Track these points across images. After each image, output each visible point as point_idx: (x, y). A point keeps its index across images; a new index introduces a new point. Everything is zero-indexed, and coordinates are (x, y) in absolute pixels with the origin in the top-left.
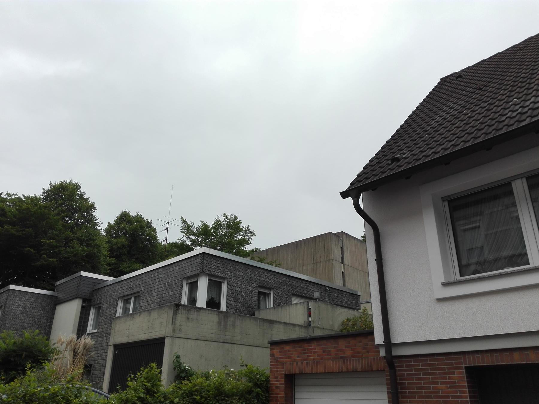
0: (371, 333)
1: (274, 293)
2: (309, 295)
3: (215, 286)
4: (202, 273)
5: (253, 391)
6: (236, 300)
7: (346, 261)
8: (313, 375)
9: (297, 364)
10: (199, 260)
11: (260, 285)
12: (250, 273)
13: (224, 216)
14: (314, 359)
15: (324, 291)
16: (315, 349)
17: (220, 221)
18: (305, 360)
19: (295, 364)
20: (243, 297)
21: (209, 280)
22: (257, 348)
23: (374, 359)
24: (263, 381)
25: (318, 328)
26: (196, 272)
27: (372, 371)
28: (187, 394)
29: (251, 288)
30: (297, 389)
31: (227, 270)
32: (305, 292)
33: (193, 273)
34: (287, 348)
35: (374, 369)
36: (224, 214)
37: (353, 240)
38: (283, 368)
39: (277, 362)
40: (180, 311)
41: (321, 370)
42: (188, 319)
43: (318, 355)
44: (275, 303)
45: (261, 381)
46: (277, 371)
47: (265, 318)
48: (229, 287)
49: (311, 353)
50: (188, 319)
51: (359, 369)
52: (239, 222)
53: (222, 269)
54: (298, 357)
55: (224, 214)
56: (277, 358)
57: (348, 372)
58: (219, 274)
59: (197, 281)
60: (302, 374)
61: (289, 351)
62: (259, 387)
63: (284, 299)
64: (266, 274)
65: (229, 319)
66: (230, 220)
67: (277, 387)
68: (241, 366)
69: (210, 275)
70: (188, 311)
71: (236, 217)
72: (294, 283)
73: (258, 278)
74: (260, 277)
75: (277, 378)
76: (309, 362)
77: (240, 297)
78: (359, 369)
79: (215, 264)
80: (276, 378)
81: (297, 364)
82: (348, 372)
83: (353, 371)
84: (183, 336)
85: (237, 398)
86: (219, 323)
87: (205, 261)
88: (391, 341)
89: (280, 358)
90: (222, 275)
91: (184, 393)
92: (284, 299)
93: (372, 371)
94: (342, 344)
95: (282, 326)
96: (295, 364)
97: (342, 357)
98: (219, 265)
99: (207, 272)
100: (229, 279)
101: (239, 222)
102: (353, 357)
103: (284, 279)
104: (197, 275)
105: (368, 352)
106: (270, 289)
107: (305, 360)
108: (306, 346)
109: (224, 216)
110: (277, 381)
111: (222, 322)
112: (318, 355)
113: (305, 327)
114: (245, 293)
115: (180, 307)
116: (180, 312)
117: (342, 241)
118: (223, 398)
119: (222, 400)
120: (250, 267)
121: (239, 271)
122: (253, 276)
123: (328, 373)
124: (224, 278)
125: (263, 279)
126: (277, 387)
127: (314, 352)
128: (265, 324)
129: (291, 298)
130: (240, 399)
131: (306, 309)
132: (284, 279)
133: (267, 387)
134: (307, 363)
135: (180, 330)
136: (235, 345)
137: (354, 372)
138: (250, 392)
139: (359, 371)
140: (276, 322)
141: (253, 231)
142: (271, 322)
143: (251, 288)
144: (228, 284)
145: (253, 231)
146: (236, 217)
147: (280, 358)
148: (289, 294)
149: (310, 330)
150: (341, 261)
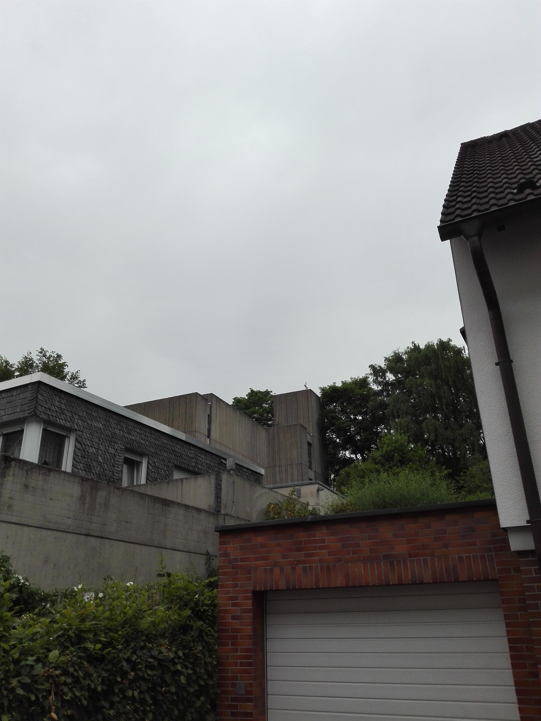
0: (491, 507)
1: (148, 463)
2: (198, 468)
3: (52, 442)
4: (34, 417)
5: (191, 627)
6: (88, 468)
7: (213, 435)
8: (294, 591)
9: (282, 569)
10: (28, 395)
11: (129, 446)
12: (114, 425)
13: (41, 353)
14: (321, 561)
15: (218, 464)
16: (323, 541)
17: (31, 359)
18: (299, 562)
19: (277, 570)
20: (100, 464)
21: (44, 429)
22: (143, 547)
23: (461, 558)
24: (207, 605)
25: (231, 516)
26: (22, 415)
27: (457, 581)
28: (69, 636)
29: (113, 451)
30: (270, 620)
31: (77, 417)
32: (193, 464)
33: (16, 416)
34: (259, 539)
35: (463, 576)
36: (42, 349)
37: (225, 406)
38: (249, 579)
39: (234, 567)
40: (11, 469)
41: (339, 581)
42: (26, 486)
43: (330, 554)
44: (150, 478)
45: (204, 605)
46: (236, 586)
47: (157, 495)
48: (78, 446)
49: (315, 548)
50: (26, 486)
51: (428, 577)
52: (64, 365)
53: (69, 414)
54: (284, 557)
55: (42, 349)
56: (236, 560)
57: (400, 584)
58: (62, 422)
59: (22, 431)
60: (294, 589)
61: (262, 546)
62: (200, 618)
63: (162, 472)
64: (138, 431)
65: (99, 494)
66: (49, 358)
67: (234, 618)
68: (160, 575)
69: (46, 422)
70: (27, 471)
71: (59, 356)
72: (178, 448)
73: (126, 435)
74: (129, 433)
75: (236, 598)
76: (311, 568)
77: (95, 464)
78: (428, 577)
79: (57, 404)
80: (231, 598)
81: (282, 569)
82: (400, 584)
83: (414, 584)
84: (14, 519)
85: (166, 641)
86: (82, 499)
87: (40, 397)
88: (499, 525)
89: (242, 560)
90: (68, 425)
91: (63, 635)
92: (162, 472)
93: (457, 581)
94: (386, 531)
95: (181, 511)
96: (277, 570)
97: (386, 557)
98: (63, 407)
99: (43, 416)
100: (78, 432)
101: (64, 365)
102: (410, 556)
103: (165, 441)
104: (23, 421)
105: (446, 546)
106: (142, 455)
107: (299, 562)
108: (302, 536)
109: (41, 353)
110: (234, 605)
111: (88, 499)
112: (330, 554)
113: (214, 514)
114: (104, 459)
115: (13, 463)
116: (11, 473)
117: (211, 406)
118: (142, 644)
119: (143, 648)
120: (114, 417)
121: (96, 421)
122: (117, 431)
123: (354, 587)
124: (70, 430)
125: (133, 438)
126: (234, 618)
127: (321, 548)
128: (157, 505)
129: (172, 472)
130: (171, 644)
131: (213, 485)
132: (165, 441)
133: (213, 617)
134: (305, 569)
135: (10, 507)
136: (107, 540)
137: (417, 584)
138: (185, 628)
139: (283, 590)
140: (173, 503)
141: (84, 381)
142: (166, 503)
143: (113, 451)
144: (76, 440)
145: (84, 381)
146: (59, 356)
147: (242, 560)
148: (170, 465)
149: (221, 519)
150: (206, 434)
